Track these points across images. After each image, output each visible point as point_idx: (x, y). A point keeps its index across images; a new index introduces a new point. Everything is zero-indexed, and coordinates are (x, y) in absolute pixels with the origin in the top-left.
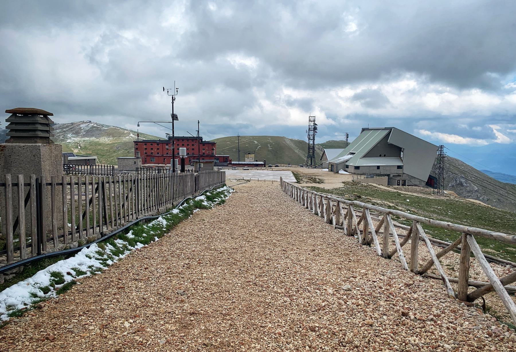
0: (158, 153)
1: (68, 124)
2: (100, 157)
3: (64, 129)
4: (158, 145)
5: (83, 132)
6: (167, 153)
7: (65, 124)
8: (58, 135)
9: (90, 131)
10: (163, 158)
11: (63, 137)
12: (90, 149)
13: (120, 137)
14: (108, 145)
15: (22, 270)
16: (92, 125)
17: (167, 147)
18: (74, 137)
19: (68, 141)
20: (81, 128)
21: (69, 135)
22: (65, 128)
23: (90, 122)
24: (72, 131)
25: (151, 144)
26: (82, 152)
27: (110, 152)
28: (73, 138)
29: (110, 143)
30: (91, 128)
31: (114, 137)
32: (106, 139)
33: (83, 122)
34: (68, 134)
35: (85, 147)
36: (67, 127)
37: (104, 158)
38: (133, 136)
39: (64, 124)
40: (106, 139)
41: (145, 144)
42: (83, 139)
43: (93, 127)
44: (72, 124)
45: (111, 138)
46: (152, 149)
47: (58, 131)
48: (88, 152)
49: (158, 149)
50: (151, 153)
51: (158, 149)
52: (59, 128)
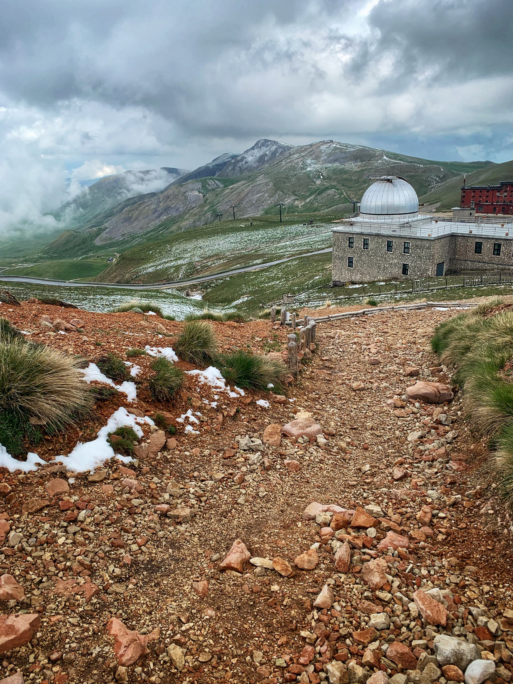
0: (487, 202)
1: (306, 146)
2: (347, 189)
3: (302, 154)
4: (488, 192)
5: (324, 157)
6: (498, 201)
7: (303, 147)
8: (297, 161)
9: (332, 154)
10: (493, 207)
11: (302, 164)
12: (334, 180)
13: (369, 161)
14: (356, 172)
15: (22, 332)
16: (335, 145)
17: (498, 194)
18: (314, 164)
19: (308, 170)
20: (321, 150)
21: (308, 162)
22: (303, 151)
23: (332, 141)
24: (311, 155)
25: (480, 192)
26: (326, 183)
27: (358, 182)
28: (313, 165)
29: (358, 170)
30: (333, 150)
31: (362, 161)
32: (353, 164)
33: (324, 143)
34: (307, 160)
35: (328, 176)
36: (306, 150)
37: (352, 191)
38: (387, 159)
39: (302, 147)
40: (353, 164)
41: (474, 192)
42: (325, 165)
43: (336, 148)
44: (311, 145)
45: (359, 164)
46: (480, 197)
47: (296, 156)
48: (333, 184)
49: (487, 197)
50: (479, 201)
51: (487, 197)
52: (296, 152)
